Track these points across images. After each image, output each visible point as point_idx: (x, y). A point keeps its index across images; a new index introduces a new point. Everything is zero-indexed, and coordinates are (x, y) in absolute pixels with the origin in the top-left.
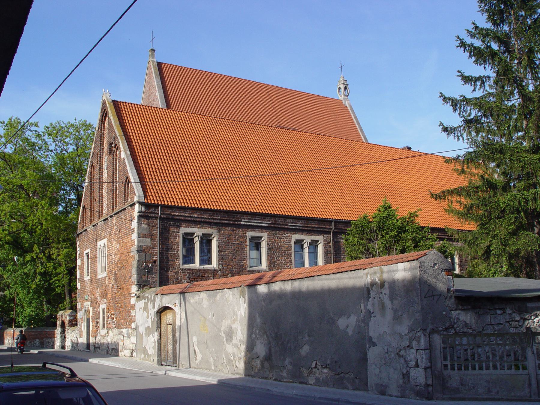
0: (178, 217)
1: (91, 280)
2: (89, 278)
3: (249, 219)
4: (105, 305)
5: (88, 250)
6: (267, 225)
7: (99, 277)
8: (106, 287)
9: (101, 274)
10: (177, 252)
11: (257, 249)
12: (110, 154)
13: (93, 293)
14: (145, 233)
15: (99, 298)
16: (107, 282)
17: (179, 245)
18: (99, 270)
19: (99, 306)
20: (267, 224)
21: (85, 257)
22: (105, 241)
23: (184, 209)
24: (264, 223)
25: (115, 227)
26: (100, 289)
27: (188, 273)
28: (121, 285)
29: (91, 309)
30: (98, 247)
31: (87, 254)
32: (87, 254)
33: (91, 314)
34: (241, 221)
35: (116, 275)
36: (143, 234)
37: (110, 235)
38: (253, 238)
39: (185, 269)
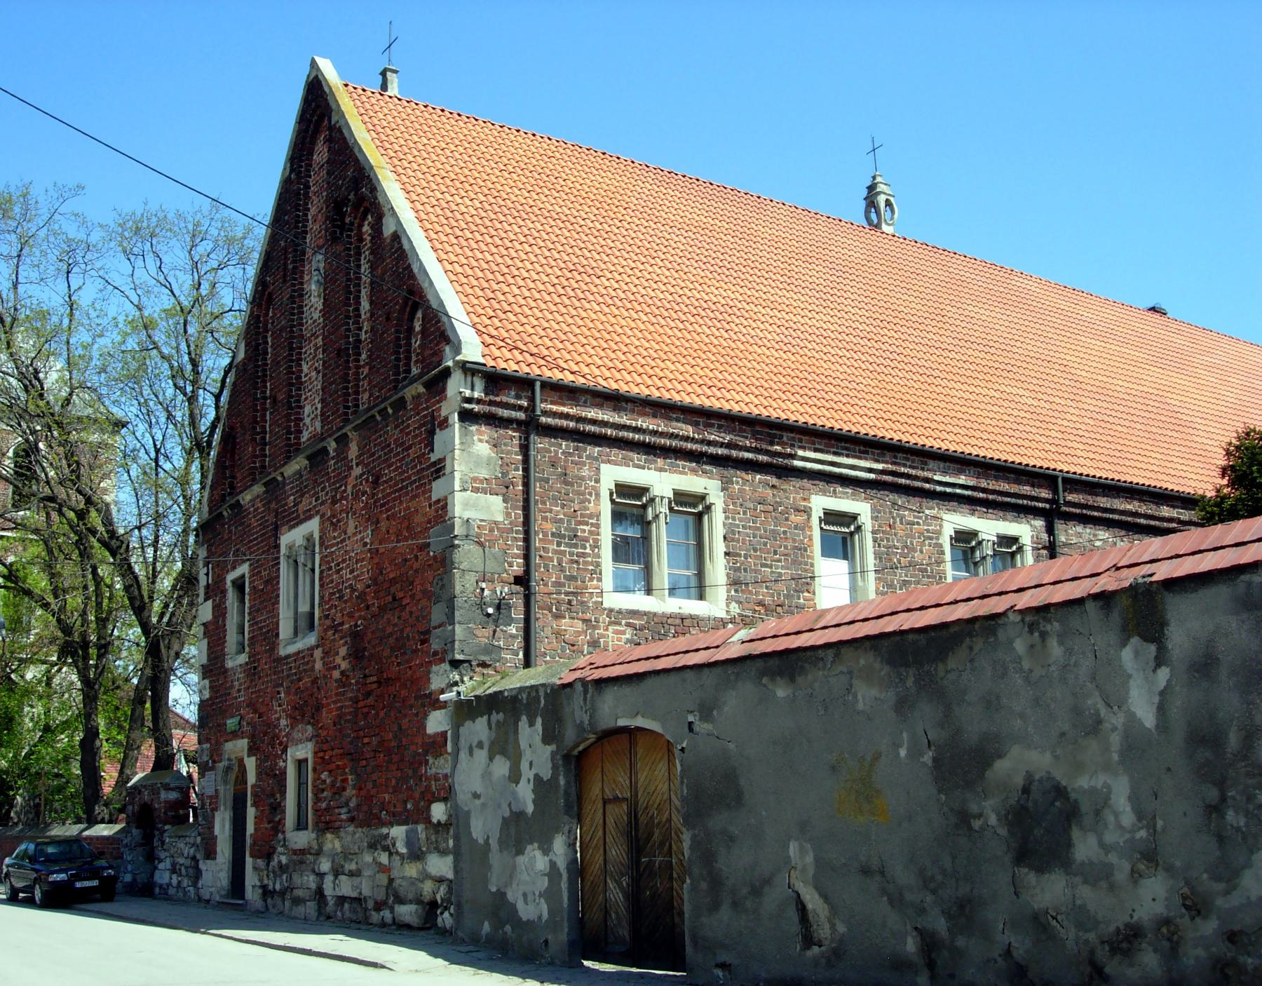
0: (593, 428)
1: (251, 670)
2: (243, 658)
3: (816, 450)
4: (310, 745)
5: (244, 569)
6: (872, 476)
7: (286, 650)
8: (315, 681)
9: (290, 643)
10: (592, 547)
11: (845, 557)
12: (334, 239)
13: (262, 709)
14: (484, 473)
15: (283, 722)
16: (318, 665)
17: (598, 526)
18: (285, 629)
19: (285, 751)
20: (870, 470)
21: (231, 595)
22: (313, 526)
23: (614, 400)
24: (862, 467)
25: (357, 471)
26: (288, 693)
27: (628, 625)
28: (381, 671)
29: (251, 763)
30: (283, 550)
31: (239, 585)
32: (239, 585)
33: (251, 778)
34: (793, 456)
35: (356, 636)
36: (475, 479)
37: (334, 502)
38: (831, 517)
39: (620, 612)
